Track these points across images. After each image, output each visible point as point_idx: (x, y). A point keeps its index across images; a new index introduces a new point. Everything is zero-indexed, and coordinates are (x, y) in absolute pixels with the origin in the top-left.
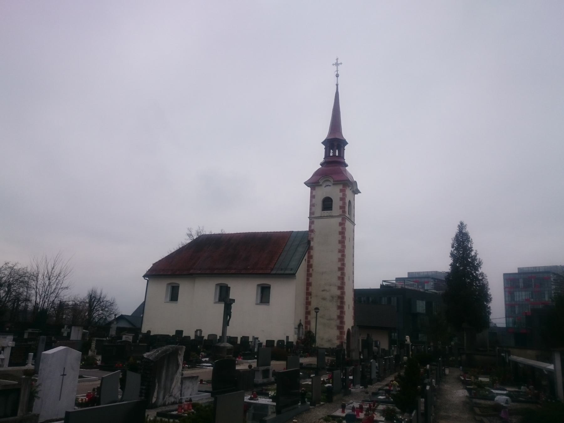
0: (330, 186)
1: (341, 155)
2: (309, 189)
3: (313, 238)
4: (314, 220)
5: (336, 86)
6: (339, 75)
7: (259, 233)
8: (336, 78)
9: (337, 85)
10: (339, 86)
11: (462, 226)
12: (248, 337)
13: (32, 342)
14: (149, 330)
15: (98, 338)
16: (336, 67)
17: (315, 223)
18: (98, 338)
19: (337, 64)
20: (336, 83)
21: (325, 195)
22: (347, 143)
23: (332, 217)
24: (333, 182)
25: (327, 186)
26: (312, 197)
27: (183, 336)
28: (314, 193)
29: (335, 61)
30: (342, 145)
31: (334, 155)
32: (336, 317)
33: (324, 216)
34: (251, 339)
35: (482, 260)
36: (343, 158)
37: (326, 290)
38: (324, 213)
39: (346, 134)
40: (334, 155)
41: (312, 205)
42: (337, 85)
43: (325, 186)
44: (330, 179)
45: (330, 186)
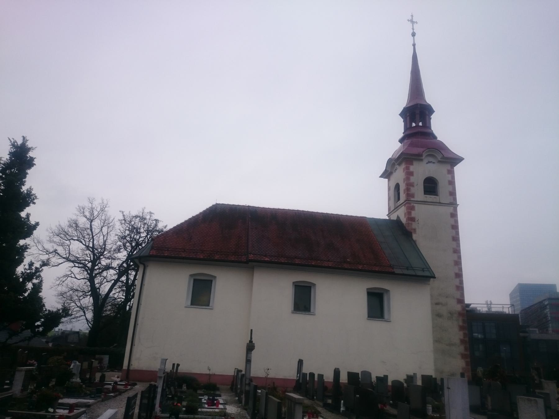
0: (434, 163)
1: (427, 125)
3: (415, 230)
4: (415, 205)
5: (413, 47)
7: (353, 216)
8: (413, 37)
9: (414, 45)
10: (416, 46)
13: (159, 409)
14: (315, 373)
15: (159, 390)
16: (412, 24)
18: (159, 390)
19: (412, 22)
20: (412, 43)
21: (427, 175)
22: (434, 112)
23: (440, 204)
25: (430, 162)
27: (390, 383)
28: (390, 185)
29: (410, 18)
30: (427, 113)
31: (417, 126)
32: (458, 342)
33: (436, 203)
35: (110, 216)
36: (429, 127)
37: (442, 304)
40: (417, 126)
42: (414, 45)
44: (436, 155)
45: (434, 163)
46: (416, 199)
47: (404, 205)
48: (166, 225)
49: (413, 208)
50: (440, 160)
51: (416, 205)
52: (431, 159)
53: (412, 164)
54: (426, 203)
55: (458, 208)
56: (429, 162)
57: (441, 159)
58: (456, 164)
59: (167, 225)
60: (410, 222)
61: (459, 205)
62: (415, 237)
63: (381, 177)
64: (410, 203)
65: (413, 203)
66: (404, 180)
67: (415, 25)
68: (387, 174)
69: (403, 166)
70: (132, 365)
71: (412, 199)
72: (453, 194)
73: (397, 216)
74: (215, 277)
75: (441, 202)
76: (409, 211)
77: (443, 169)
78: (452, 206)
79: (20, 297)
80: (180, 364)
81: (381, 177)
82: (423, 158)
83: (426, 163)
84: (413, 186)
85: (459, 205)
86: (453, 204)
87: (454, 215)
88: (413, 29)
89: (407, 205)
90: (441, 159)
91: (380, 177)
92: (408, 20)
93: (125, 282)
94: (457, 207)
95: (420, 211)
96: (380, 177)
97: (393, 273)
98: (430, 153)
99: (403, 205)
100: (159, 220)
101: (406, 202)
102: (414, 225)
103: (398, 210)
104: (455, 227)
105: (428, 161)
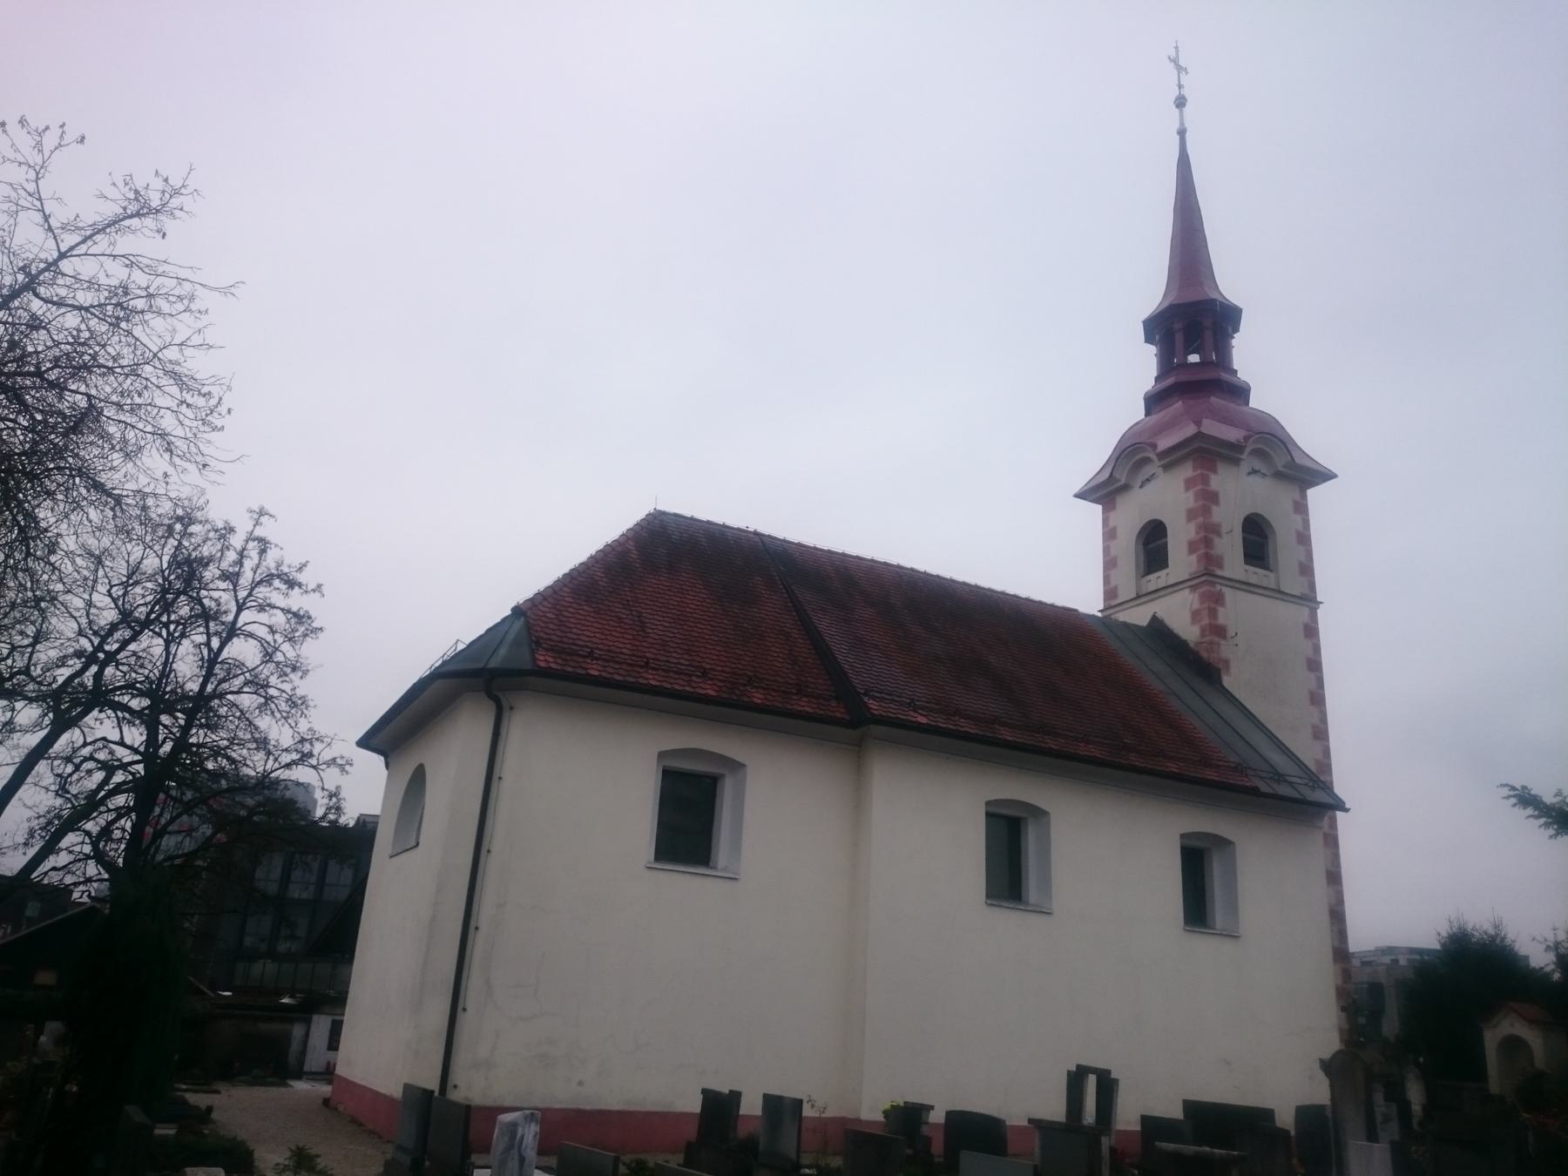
0: (1264, 475)
2: (1099, 508)
4: (1225, 589)
6: (1177, 106)
8: (1177, 110)
9: (1182, 133)
10: (1188, 135)
11: (1333, 476)
12: (735, 1097)
17: (289, 562)
20: (1177, 126)
24: (1159, 460)
26: (1110, 534)
28: (1112, 524)
33: (1265, 588)
34: (751, 1106)
38: (1265, 576)
39: (1231, 281)
41: (1110, 564)
42: (1182, 133)
43: (1140, 484)
44: (1272, 453)
46: (1227, 573)
47: (1191, 587)
48: (304, 561)
49: (1218, 599)
50: (1281, 469)
51: (1228, 592)
52: (1258, 465)
53: (1215, 471)
54: (1252, 589)
55: (1318, 611)
56: (1254, 472)
57: (1284, 467)
58: (1312, 484)
59: (307, 562)
60: (1216, 639)
61: (1321, 603)
62: (1227, 681)
63: (1081, 495)
64: (1213, 584)
65: (1220, 584)
66: (1191, 515)
67: (184, 209)
68: (1104, 491)
69: (1187, 471)
70: (455, 1087)
71: (1219, 572)
72: (1307, 570)
73: (1152, 614)
74: (736, 766)
75: (1283, 589)
76: (1212, 605)
77: (1286, 494)
78: (1307, 606)
79: (106, 788)
80: (700, 1091)
81: (1081, 495)
82: (1244, 456)
83: (1138, 486)
84: (1219, 534)
85: (1321, 603)
86: (1309, 599)
87: (1311, 631)
88: (1180, 86)
89: (1205, 589)
90: (1284, 467)
91: (1077, 496)
92: (1169, 58)
93: (142, 749)
94: (1316, 609)
95: (1239, 610)
96: (1077, 496)
97: (1255, 792)
98: (1138, 457)
99: (1184, 585)
100: (273, 540)
101: (1203, 579)
102: (1225, 650)
103: (1153, 600)
104: (1314, 665)
105: (1253, 469)
